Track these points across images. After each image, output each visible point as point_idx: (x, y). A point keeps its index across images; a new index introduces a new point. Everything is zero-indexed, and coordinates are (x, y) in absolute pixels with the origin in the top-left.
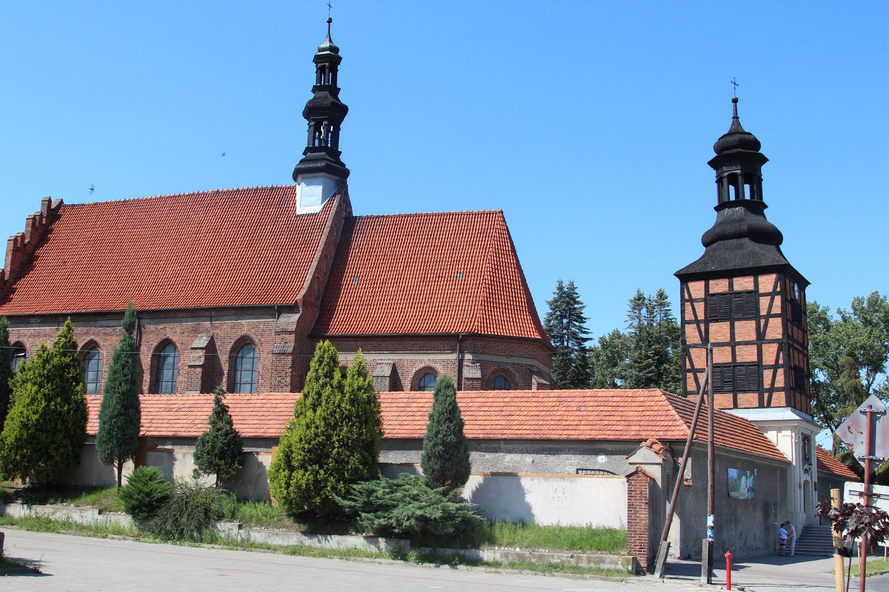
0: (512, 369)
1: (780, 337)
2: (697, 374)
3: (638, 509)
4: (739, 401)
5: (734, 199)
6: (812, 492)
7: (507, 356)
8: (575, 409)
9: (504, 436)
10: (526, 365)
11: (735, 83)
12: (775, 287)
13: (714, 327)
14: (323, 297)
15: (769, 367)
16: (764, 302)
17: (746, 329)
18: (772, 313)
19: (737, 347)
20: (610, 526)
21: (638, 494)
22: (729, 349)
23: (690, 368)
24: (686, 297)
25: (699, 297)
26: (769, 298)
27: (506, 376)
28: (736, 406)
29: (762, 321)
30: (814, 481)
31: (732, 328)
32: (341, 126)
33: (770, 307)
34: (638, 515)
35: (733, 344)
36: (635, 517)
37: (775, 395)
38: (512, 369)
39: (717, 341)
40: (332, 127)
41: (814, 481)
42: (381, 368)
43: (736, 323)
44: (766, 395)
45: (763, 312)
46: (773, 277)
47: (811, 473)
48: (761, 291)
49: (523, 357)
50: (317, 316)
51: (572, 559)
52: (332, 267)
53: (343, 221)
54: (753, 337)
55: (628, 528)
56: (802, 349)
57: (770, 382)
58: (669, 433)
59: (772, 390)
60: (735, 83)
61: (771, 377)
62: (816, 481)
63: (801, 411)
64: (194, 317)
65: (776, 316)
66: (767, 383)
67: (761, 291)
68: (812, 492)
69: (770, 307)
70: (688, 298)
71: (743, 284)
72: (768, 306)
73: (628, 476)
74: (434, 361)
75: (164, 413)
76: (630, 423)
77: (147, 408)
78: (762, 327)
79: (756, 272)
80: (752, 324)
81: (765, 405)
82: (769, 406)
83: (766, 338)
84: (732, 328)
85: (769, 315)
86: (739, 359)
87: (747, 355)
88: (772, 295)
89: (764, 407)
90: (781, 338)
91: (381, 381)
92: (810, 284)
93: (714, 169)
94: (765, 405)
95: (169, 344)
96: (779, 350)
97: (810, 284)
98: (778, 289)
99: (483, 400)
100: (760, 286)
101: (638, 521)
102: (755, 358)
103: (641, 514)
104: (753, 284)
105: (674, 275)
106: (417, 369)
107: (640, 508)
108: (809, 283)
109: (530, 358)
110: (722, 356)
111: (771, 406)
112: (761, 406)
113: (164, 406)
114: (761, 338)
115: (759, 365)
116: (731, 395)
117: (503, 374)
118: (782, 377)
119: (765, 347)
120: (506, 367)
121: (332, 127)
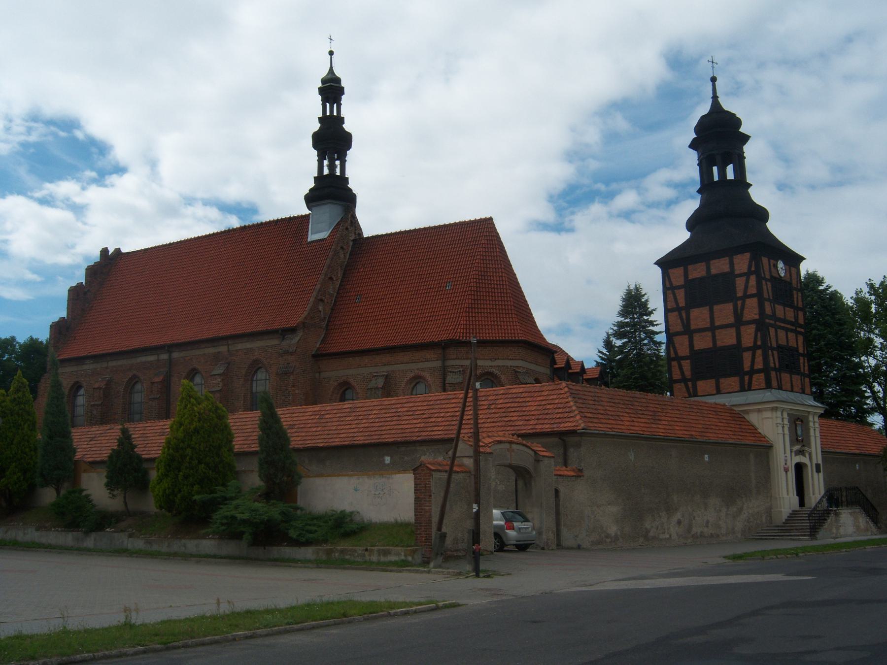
0: (497, 372)
1: (757, 317)
2: (682, 361)
3: (423, 502)
4: (721, 386)
5: (733, 178)
6: (812, 474)
7: (491, 359)
8: (486, 407)
9: (419, 439)
10: (511, 366)
11: (712, 62)
12: (750, 266)
13: (695, 313)
14: (329, 317)
15: (748, 349)
16: (740, 283)
17: (724, 313)
18: (748, 294)
19: (716, 331)
20: (403, 519)
21: (423, 487)
22: (709, 334)
23: (674, 356)
24: (668, 283)
25: (679, 284)
26: (744, 278)
27: (492, 379)
28: (719, 392)
29: (739, 303)
30: (814, 462)
31: (711, 312)
32: (316, 152)
33: (746, 287)
34: (423, 508)
35: (713, 328)
36: (420, 509)
37: (755, 377)
38: (497, 372)
39: (698, 327)
40: (336, 155)
41: (814, 462)
42: (376, 380)
43: (715, 307)
44: (746, 378)
45: (740, 294)
46: (747, 255)
47: (810, 454)
48: (737, 272)
49: (508, 359)
50: (323, 336)
51: (366, 553)
52: (339, 289)
53: (351, 243)
54: (731, 320)
55: (415, 520)
56: (794, 328)
57: (749, 364)
58: (562, 425)
59: (752, 372)
60: (712, 62)
61: (750, 359)
62: (820, 462)
63: (792, 391)
64: (214, 347)
65: (752, 296)
66: (747, 366)
67: (737, 272)
68: (812, 474)
69: (746, 287)
70: (669, 286)
71: (720, 266)
72: (743, 286)
73: (414, 470)
74: (423, 370)
75: (158, 438)
76: (530, 418)
77: (147, 433)
78: (739, 308)
79: (730, 252)
80: (729, 307)
81: (746, 387)
82: (750, 389)
83: (744, 319)
84: (711, 312)
85: (746, 296)
86: (719, 343)
87: (727, 338)
88: (747, 275)
89: (745, 391)
90: (758, 318)
91: (375, 393)
92: (804, 259)
93: (696, 150)
94: (746, 387)
95: (196, 373)
96: (757, 330)
97: (804, 259)
98: (753, 269)
99: (411, 405)
100: (736, 267)
101: (423, 513)
102: (733, 341)
103: (425, 506)
104: (728, 266)
105: (656, 263)
106: (408, 378)
107: (424, 501)
108: (803, 259)
109: (515, 359)
110: (702, 342)
111: (752, 389)
112: (743, 389)
113: (159, 431)
114: (739, 322)
115: (737, 349)
116: (713, 381)
117: (489, 377)
118: (761, 358)
119: (743, 328)
120: (490, 370)
121: (336, 155)
